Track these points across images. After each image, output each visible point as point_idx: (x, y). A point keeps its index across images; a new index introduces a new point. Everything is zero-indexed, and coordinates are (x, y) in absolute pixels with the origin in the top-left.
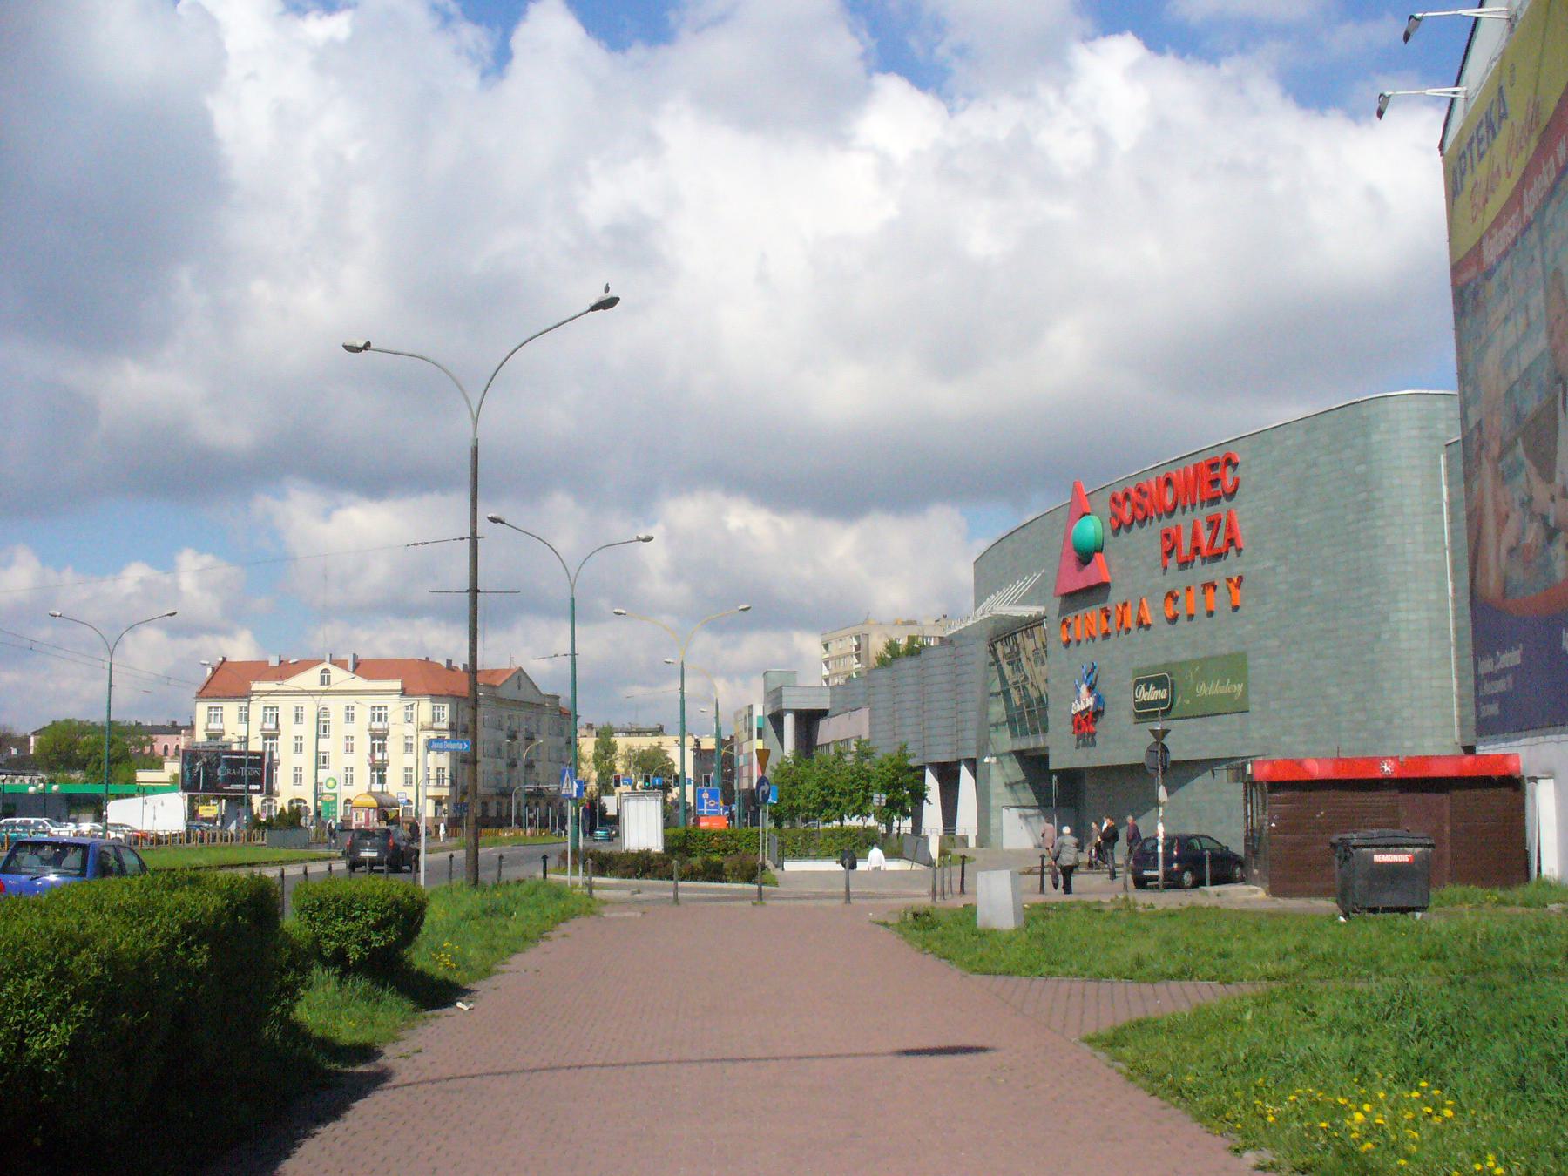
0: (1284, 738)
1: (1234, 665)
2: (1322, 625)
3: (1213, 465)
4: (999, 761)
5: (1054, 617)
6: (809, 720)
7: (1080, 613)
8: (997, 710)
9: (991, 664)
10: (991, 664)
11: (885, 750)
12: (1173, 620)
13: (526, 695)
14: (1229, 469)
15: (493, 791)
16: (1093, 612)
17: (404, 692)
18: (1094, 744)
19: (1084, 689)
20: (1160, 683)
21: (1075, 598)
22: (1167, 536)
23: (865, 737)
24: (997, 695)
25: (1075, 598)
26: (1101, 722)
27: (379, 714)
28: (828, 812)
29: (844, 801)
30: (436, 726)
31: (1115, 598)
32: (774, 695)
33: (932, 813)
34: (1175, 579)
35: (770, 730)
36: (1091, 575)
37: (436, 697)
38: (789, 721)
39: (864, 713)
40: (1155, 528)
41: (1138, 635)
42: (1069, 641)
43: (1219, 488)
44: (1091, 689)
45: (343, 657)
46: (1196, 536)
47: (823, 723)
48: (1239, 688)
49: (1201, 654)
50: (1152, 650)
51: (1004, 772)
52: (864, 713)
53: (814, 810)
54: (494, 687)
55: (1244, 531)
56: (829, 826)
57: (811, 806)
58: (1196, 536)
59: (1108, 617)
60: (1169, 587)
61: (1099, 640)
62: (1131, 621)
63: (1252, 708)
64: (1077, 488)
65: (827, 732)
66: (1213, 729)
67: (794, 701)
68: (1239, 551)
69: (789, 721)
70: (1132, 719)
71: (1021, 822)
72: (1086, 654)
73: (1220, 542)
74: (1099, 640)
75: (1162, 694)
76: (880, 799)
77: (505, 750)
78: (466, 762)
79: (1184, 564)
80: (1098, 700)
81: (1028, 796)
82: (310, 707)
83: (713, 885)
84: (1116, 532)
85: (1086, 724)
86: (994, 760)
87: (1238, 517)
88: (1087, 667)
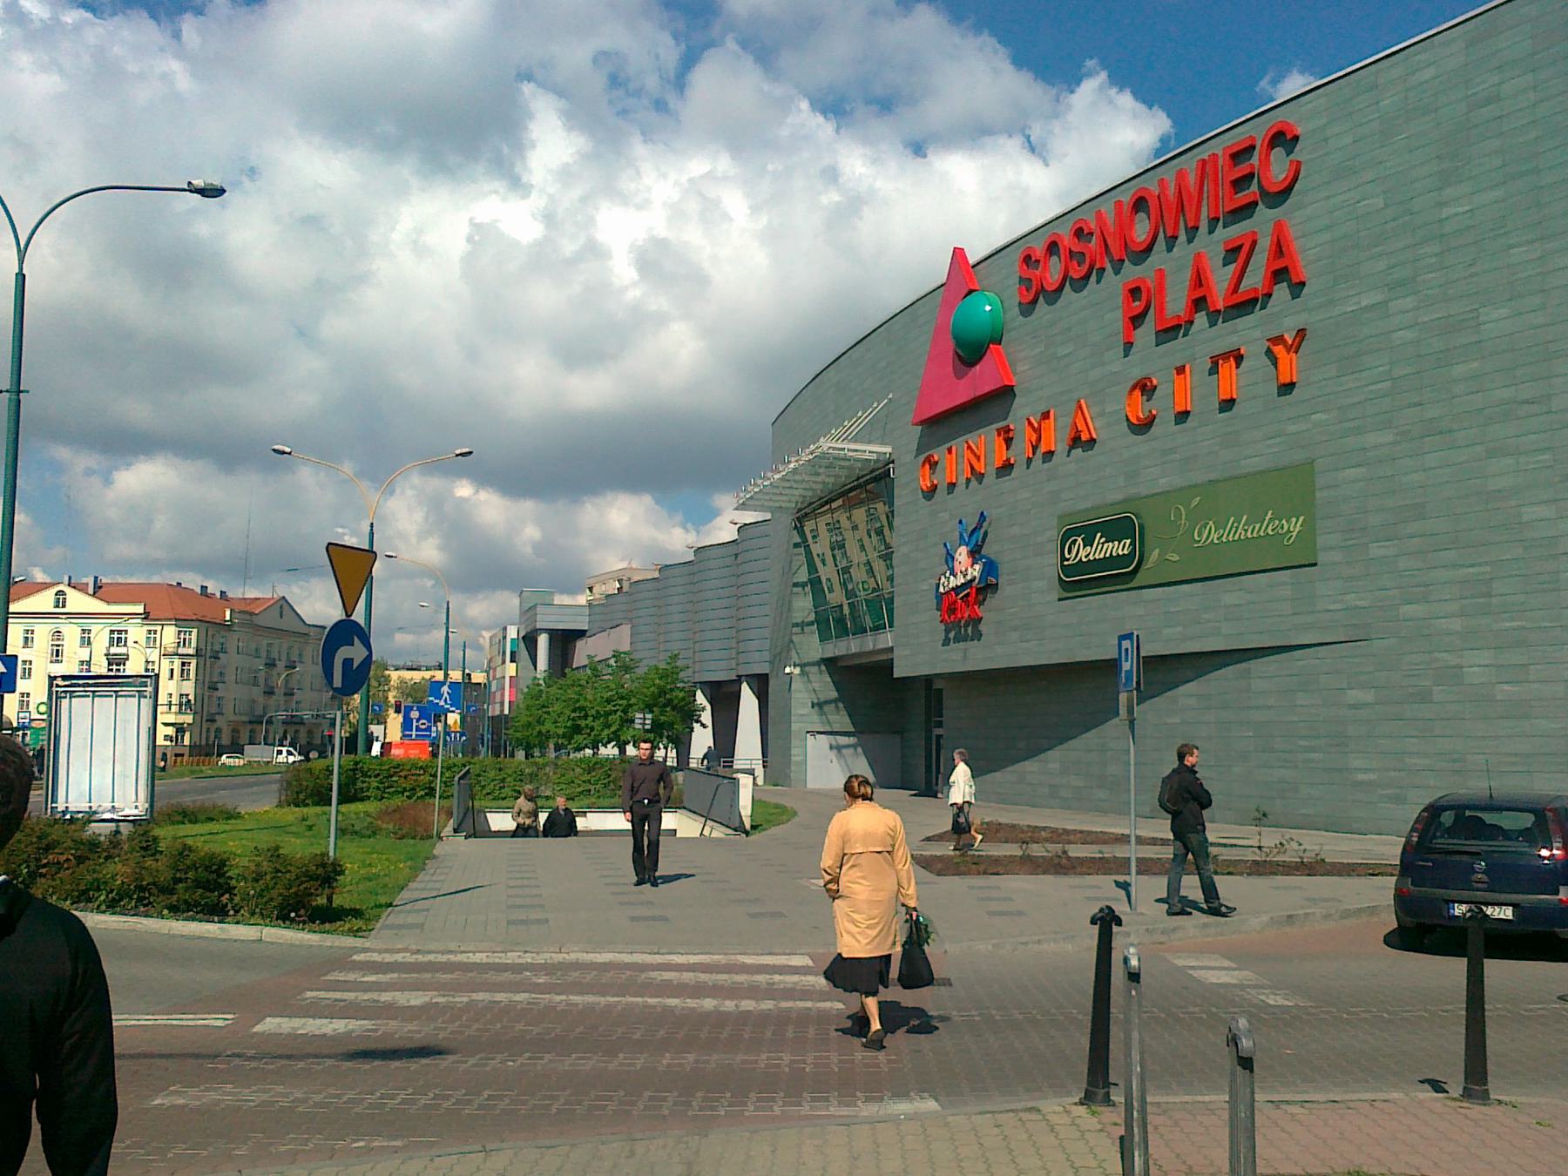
0: (1407, 610)
1: (1293, 485)
2: (1508, 393)
3: (1241, 154)
4: (803, 673)
5: (909, 457)
6: (564, 641)
7: (958, 444)
8: (803, 605)
9: (796, 545)
10: (796, 545)
11: (650, 660)
12: (1143, 426)
13: (288, 623)
14: (1278, 153)
15: (245, 719)
16: (985, 439)
17: (146, 616)
18: (978, 635)
19: (962, 554)
20: (1117, 528)
21: (940, 424)
22: (1134, 292)
23: (626, 647)
24: (803, 585)
25: (940, 424)
26: (992, 601)
27: (118, 638)
28: (579, 738)
29: (597, 724)
30: (181, 651)
31: (1021, 413)
32: (529, 612)
33: (702, 740)
34: (1150, 357)
35: (523, 653)
36: (982, 379)
37: (179, 621)
38: (543, 641)
39: (626, 630)
40: (1110, 289)
41: (1068, 463)
42: (934, 488)
43: (1254, 187)
44: (975, 554)
45: (84, 580)
46: (1199, 280)
47: (580, 644)
48: (1295, 526)
49: (1199, 477)
50: (1093, 484)
51: (805, 691)
52: (626, 630)
53: (564, 736)
54: (252, 614)
55: (1308, 255)
56: (579, 755)
57: (560, 732)
58: (1199, 280)
59: (1008, 442)
60: (1137, 374)
61: (990, 478)
62: (1056, 437)
63: (1322, 558)
64: (959, 254)
65: (583, 652)
66: (1229, 599)
67: (547, 620)
68: (1298, 287)
69: (543, 641)
70: (1057, 592)
71: (833, 755)
72: (967, 503)
73: (1255, 278)
74: (990, 478)
75: (1120, 548)
76: (643, 720)
77: (261, 675)
78: (208, 686)
79: (1170, 331)
80: (990, 568)
81: (842, 720)
82: (43, 630)
83: (211, 929)
84: (1028, 308)
85: (962, 610)
86: (797, 671)
87: (1293, 231)
88: (971, 522)
